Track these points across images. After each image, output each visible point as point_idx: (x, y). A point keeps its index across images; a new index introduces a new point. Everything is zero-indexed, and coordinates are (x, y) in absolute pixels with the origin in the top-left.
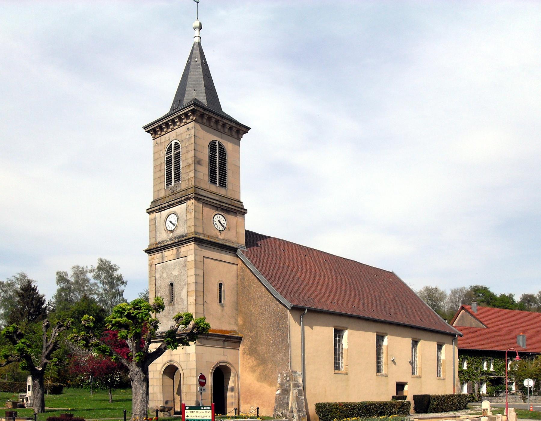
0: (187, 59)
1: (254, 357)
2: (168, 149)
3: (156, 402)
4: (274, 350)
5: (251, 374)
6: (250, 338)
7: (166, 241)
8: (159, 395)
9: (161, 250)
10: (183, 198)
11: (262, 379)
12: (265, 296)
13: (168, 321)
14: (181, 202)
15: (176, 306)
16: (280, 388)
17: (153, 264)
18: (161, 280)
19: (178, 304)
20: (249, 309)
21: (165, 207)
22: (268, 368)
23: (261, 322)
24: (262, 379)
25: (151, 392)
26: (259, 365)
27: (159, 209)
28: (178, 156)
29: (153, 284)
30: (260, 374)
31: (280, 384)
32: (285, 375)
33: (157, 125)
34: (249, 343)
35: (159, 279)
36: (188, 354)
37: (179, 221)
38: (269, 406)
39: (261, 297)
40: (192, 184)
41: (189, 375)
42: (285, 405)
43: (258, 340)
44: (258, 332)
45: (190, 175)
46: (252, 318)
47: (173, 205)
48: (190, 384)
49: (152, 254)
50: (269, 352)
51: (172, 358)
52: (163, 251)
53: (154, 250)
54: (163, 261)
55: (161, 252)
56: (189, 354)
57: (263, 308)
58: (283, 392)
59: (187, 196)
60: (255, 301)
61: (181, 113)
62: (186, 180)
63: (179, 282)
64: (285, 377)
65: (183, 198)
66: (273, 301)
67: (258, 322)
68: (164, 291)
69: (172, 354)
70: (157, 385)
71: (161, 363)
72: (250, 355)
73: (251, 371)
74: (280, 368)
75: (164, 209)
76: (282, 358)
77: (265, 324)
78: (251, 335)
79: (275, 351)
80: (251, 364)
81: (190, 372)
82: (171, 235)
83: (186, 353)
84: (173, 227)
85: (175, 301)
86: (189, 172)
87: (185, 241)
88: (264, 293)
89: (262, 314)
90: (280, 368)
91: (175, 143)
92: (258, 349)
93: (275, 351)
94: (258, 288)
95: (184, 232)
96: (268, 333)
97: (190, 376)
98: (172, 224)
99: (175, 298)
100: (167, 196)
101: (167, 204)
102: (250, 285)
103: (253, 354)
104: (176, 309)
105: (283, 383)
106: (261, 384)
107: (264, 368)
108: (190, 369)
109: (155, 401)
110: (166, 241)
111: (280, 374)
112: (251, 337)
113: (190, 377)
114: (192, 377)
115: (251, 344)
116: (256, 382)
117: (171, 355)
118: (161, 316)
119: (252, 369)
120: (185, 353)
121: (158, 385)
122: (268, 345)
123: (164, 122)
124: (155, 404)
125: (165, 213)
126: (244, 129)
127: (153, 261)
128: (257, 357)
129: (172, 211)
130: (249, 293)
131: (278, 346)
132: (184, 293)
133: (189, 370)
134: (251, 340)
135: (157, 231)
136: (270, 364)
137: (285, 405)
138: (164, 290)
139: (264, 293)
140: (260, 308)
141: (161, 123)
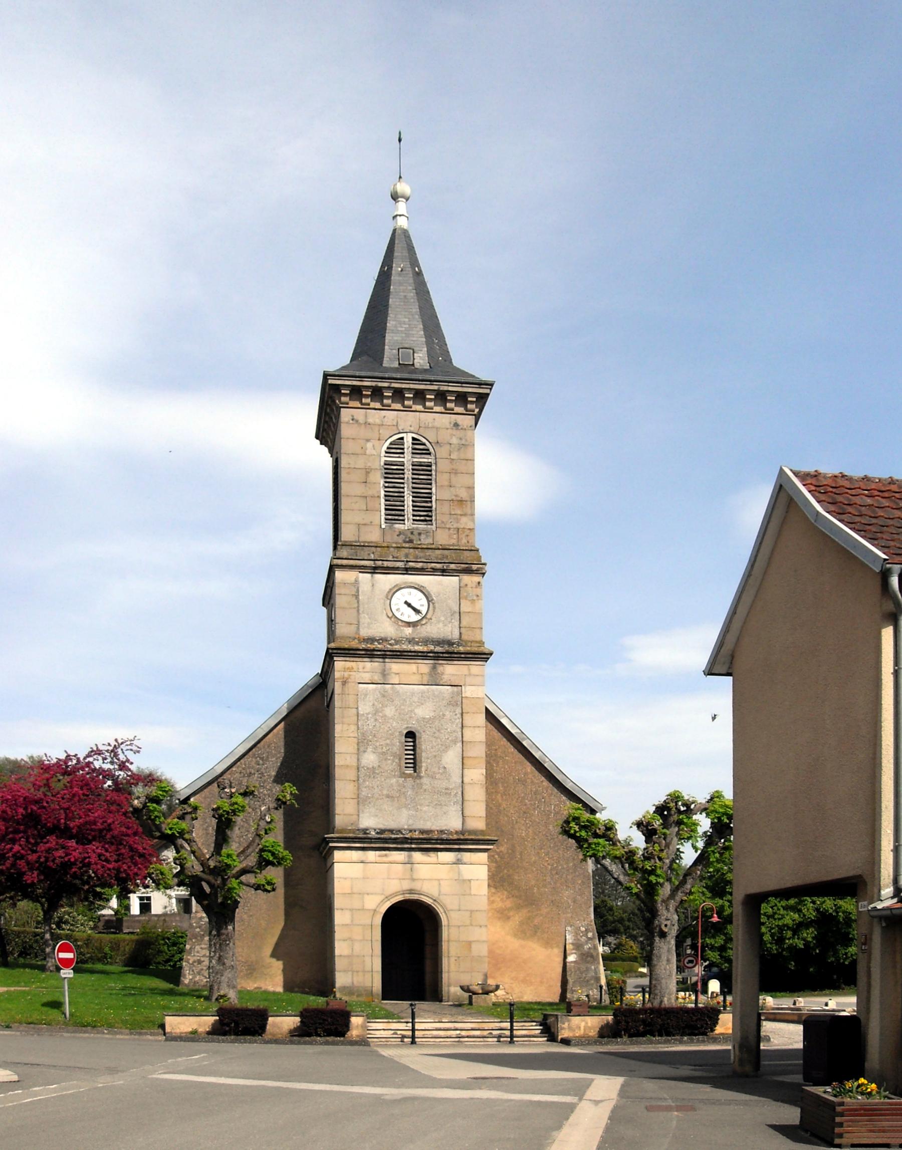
0: (422, 269)
1: (506, 893)
2: (391, 444)
3: (361, 974)
4: (555, 883)
5: (499, 924)
6: (496, 856)
7: (395, 640)
8: (368, 960)
9: (384, 657)
10: (453, 566)
11: (525, 934)
12: (532, 782)
13: (399, 808)
14: (444, 572)
15: (425, 780)
16: (574, 951)
17: (349, 680)
18: (376, 720)
19: (433, 777)
20: (493, 800)
21: (398, 568)
22: (542, 915)
23: (523, 828)
24: (525, 934)
25: (343, 954)
26: (518, 907)
27: (375, 568)
28: (423, 471)
29: (349, 724)
30: (522, 923)
31: (572, 944)
32: (583, 929)
33: (374, 384)
34: (494, 865)
35: (370, 716)
36: (464, 881)
37: (434, 607)
38: (542, 982)
39: (523, 782)
40: (468, 542)
41: (468, 922)
42: (592, 982)
43: (517, 861)
44: (516, 845)
45: (461, 522)
46: (501, 818)
47: (421, 571)
48: (471, 939)
49: (348, 659)
50: (544, 886)
51: (417, 886)
52: (387, 660)
53: (363, 652)
54: (385, 680)
55: (381, 660)
56: (470, 881)
57: (528, 803)
58: (582, 959)
59: (467, 566)
60: (508, 786)
61: (450, 389)
62: (449, 529)
63: (434, 733)
64: (582, 932)
65: (453, 566)
66: (552, 794)
67: (516, 826)
68: (387, 744)
69: (415, 877)
70: (364, 940)
71: (379, 894)
72: (496, 888)
73: (499, 919)
74: (569, 915)
75: (387, 570)
76: (574, 898)
77: (535, 833)
78: (498, 850)
79: (558, 885)
80: (499, 904)
81: (471, 917)
82: (408, 631)
83: (461, 878)
84: (417, 618)
85: (423, 769)
86: (461, 515)
87: (463, 656)
88: (530, 776)
89: (525, 813)
90: (569, 915)
91: (414, 439)
92: (516, 878)
93: (558, 885)
94: (515, 763)
95: (450, 634)
96: (541, 849)
97: (471, 925)
98: (410, 609)
99: (424, 764)
100: (394, 545)
101: (370, 563)
102: (496, 755)
103: (502, 886)
104: (425, 787)
105: (580, 942)
106: (523, 942)
107: (530, 914)
108: (472, 911)
109: (357, 972)
110: (395, 640)
111: (571, 926)
112: (498, 854)
113: (470, 927)
114: (476, 926)
115: (498, 867)
116: (509, 938)
117: (413, 880)
118: (376, 796)
119: (502, 913)
120: (457, 878)
121: (367, 940)
122: (542, 873)
123: (393, 385)
124: (355, 979)
125: (386, 581)
126: (783, 500)
127: (351, 673)
128: (513, 892)
129: (411, 583)
130: (492, 769)
131: (564, 876)
132: (451, 758)
133: (468, 913)
134: (498, 859)
135: (363, 612)
136: (546, 908)
137: (592, 982)
138: (388, 741)
139: (530, 776)
140: (521, 802)
141: (386, 385)
